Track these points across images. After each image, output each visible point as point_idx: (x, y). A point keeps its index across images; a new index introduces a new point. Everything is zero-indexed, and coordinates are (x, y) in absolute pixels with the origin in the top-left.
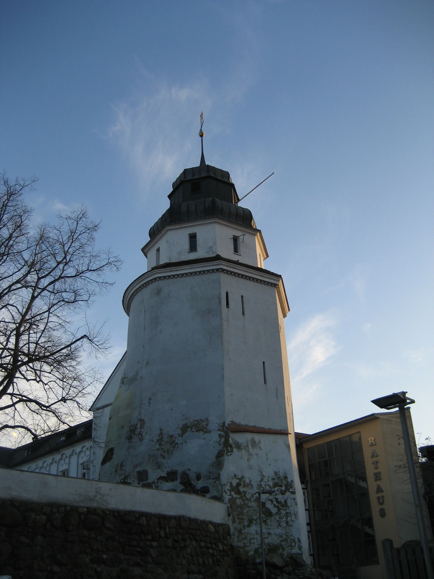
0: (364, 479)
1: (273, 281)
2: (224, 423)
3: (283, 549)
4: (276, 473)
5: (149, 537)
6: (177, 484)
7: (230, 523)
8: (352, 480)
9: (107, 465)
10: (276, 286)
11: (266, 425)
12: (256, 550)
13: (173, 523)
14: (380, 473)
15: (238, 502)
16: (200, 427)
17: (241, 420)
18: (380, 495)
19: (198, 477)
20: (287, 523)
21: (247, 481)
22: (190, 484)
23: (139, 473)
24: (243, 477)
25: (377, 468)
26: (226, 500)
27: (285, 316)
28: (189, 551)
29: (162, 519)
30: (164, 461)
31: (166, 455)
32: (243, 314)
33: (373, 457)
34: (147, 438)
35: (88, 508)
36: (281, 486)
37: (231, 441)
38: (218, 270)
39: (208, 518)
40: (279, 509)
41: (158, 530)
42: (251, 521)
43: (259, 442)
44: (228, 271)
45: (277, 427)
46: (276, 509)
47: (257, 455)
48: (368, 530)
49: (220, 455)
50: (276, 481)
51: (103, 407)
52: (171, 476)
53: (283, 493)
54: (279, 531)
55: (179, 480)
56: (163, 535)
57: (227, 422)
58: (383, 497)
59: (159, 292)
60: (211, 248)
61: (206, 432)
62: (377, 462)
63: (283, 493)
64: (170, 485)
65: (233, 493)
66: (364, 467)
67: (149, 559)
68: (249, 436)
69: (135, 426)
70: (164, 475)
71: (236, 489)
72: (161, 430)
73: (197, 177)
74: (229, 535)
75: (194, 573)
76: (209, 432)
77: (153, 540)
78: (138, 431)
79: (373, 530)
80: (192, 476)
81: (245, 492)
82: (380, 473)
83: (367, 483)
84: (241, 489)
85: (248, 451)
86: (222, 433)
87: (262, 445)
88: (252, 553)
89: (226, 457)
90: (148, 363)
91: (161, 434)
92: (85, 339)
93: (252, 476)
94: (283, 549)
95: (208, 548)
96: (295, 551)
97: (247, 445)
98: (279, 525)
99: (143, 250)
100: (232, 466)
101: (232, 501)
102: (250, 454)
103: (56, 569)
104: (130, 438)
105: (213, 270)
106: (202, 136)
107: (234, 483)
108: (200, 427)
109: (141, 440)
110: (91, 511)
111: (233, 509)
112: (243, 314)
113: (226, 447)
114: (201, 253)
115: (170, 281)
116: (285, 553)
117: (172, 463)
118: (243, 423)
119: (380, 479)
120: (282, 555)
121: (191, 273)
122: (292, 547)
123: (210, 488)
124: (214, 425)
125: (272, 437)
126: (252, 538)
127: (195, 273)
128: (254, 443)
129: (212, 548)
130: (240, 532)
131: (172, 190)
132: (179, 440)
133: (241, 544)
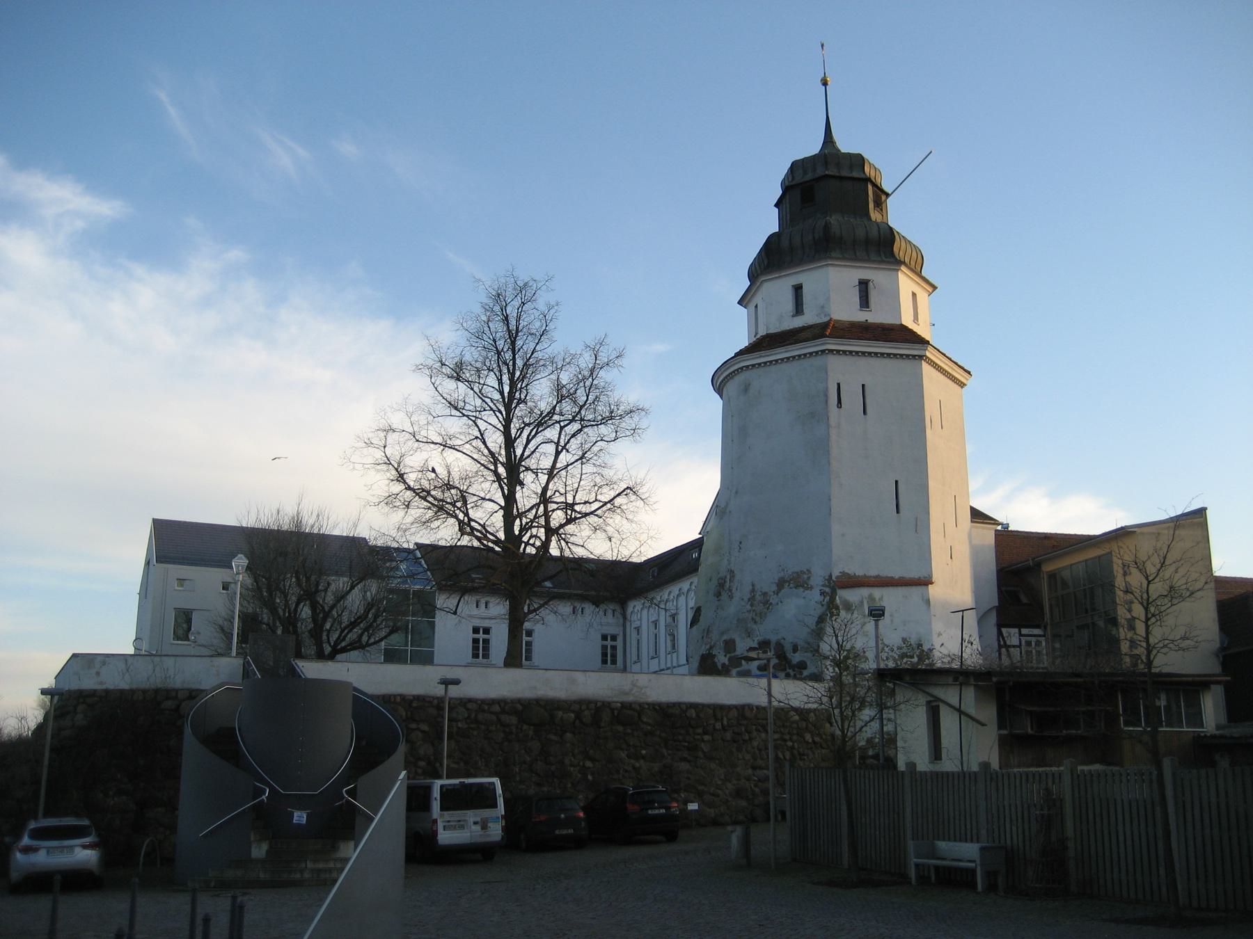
2: (831, 576)
4: (904, 640)
5: (700, 731)
11: (896, 572)
12: (869, 741)
13: (734, 713)
16: (799, 581)
17: (857, 570)
19: (795, 649)
23: (726, 642)
29: (718, 710)
31: (758, 619)
32: (865, 412)
34: (737, 595)
36: (912, 657)
37: (838, 600)
38: (823, 351)
41: (712, 722)
49: (821, 620)
56: (718, 726)
57: (836, 573)
59: (746, 388)
61: (807, 589)
67: (700, 754)
68: (865, 592)
69: (724, 579)
73: (809, 177)
76: (811, 588)
77: (705, 733)
78: (727, 585)
86: (827, 590)
95: (785, 741)
101: (837, 680)
103: (589, 764)
104: (718, 595)
106: (825, 83)
108: (799, 581)
109: (731, 597)
110: (626, 706)
112: (865, 412)
113: (831, 608)
114: (810, 317)
117: (766, 629)
118: (860, 572)
124: (817, 580)
125: (900, 591)
127: (794, 357)
129: (791, 739)
131: (780, 192)
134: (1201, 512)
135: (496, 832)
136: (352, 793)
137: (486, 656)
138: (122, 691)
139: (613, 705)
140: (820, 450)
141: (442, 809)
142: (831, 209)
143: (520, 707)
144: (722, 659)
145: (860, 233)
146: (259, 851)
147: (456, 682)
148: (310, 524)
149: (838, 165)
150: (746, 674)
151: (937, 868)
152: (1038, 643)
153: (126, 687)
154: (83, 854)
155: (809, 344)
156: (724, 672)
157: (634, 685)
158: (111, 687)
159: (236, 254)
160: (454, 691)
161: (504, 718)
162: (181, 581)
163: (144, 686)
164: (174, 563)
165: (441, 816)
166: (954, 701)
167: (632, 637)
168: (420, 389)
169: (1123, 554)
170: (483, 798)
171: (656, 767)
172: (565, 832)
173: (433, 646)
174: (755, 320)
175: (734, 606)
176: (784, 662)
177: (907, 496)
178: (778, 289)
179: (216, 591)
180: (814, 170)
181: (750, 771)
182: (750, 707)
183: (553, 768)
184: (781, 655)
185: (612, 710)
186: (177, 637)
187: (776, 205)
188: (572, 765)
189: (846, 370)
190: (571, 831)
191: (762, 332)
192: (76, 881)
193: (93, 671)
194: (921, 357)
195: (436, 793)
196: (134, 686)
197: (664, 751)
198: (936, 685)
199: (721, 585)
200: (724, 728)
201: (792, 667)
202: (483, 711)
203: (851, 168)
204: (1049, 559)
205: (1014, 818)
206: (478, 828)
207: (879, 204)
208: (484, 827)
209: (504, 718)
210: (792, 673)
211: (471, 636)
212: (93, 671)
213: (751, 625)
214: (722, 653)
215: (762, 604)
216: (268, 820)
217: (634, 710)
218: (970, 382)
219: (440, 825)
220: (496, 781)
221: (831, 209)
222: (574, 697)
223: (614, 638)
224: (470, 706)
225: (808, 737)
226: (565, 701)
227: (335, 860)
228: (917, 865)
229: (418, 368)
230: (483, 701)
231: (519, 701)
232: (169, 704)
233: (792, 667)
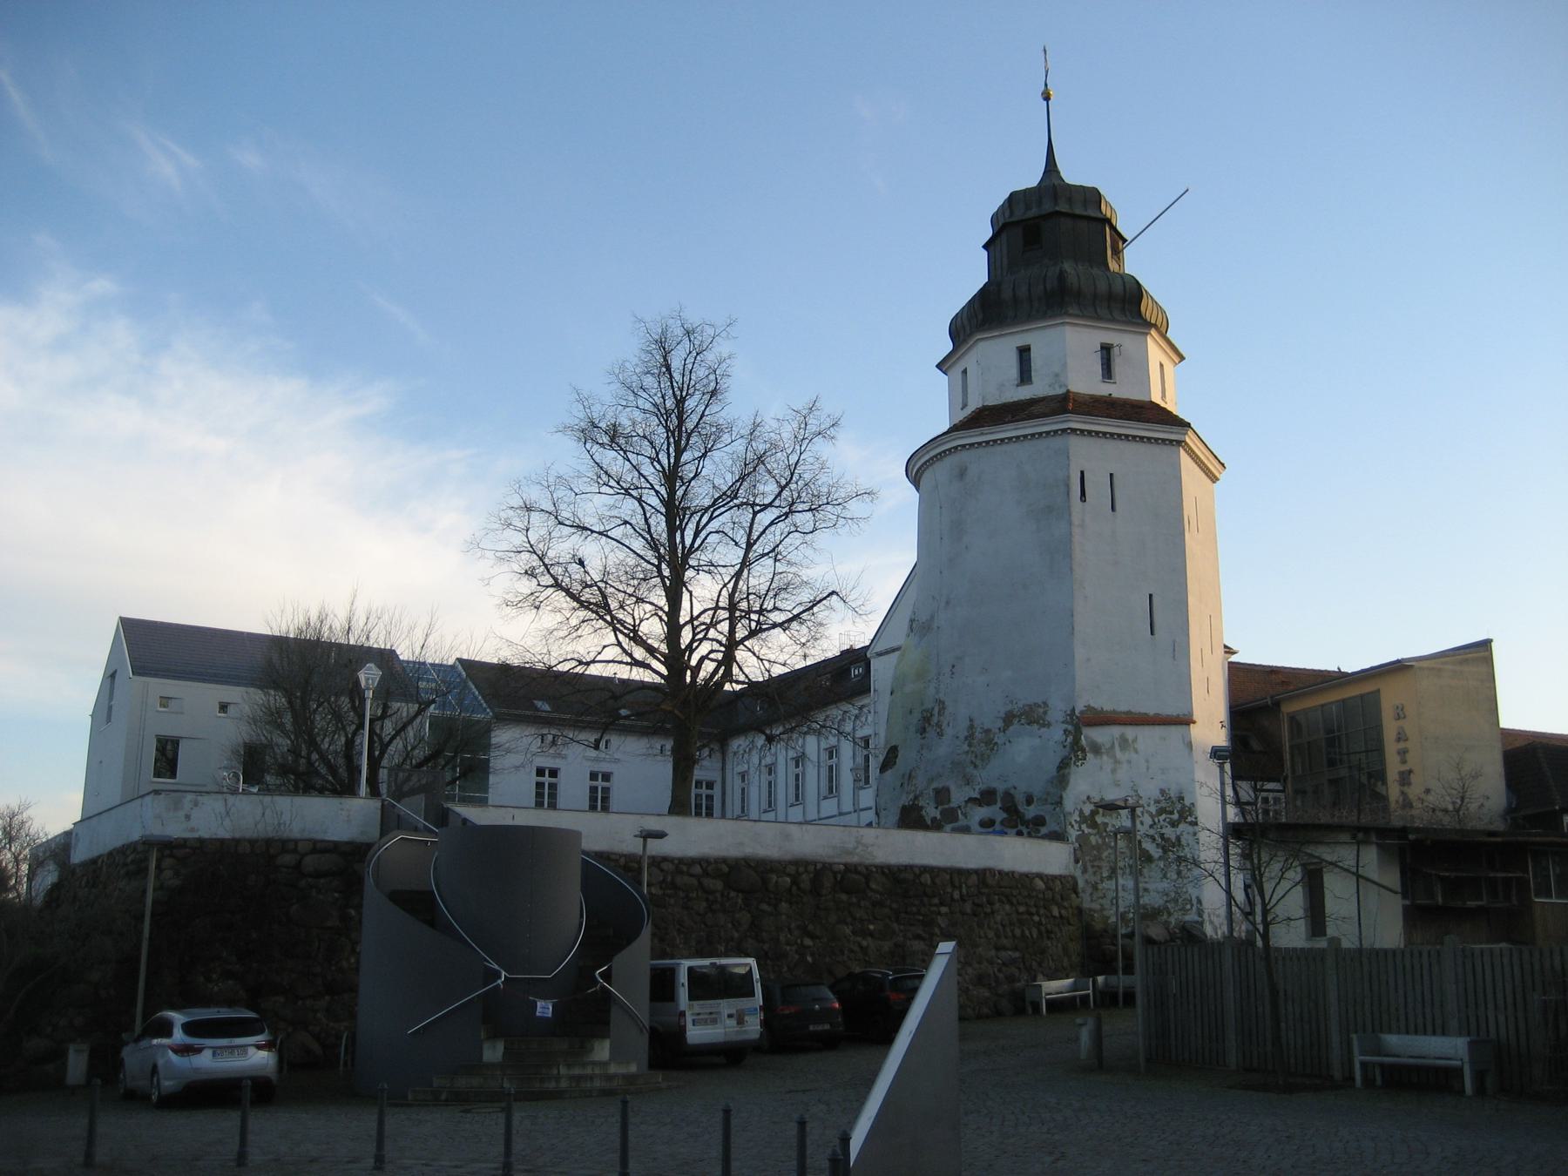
0: (1384, 782)
1: (1173, 437)
3: (1170, 914)
4: (1162, 792)
5: (936, 901)
6: (995, 812)
7: (1078, 874)
9: (889, 772)
11: (1151, 709)
15: (1093, 840)
16: (1033, 716)
17: (1105, 703)
19: (1029, 800)
22: (1017, 811)
25: (1404, 762)
26: (1073, 838)
28: (999, 918)
29: (957, 875)
30: (975, 772)
32: (1113, 509)
34: (949, 732)
35: (845, 865)
38: (1064, 431)
39: (1034, 868)
40: (1165, 851)
43: (1135, 740)
44: (1082, 431)
45: (1170, 710)
47: (1129, 762)
49: (1064, 765)
50: (1163, 805)
51: (887, 652)
52: (987, 797)
53: (1174, 824)
54: (1165, 885)
55: (999, 804)
56: (956, 895)
57: (1080, 707)
59: (962, 473)
60: (1057, 375)
61: (1044, 726)
63: (1174, 824)
64: (982, 813)
65: (1084, 827)
67: (937, 930)
68: (1116, 731)
73: (1034, 212)
74: (1076, 893)
75: (1005, 948)
76: (1049, 725)
77: (942, 904)
78: (935, 719)
80: (1020, 798)
81: (1106, 825)
86: (1070, 728)
87: (1140, 745)
90: (948, 603)
91: (971, 727)
92: (835, 597)
94: (1170, 914)
95: (1031, 914)
96: (1191, 917)
98: (1165, 876)
100: (1086, 784)
101: (1083, 839)
102: (1117, 762)
103: (808, 942)
106: (1047, 98)
107: (1087, 809)
108: (1033, 716)
109: (940, 734)
110: (850, 869)
112: (1113, 509)
114: (1040, 387)
115: (981, 451)
116: (1173, 920)
117: (988, 776)
118: (1108, 707)
119: (1409, 784)
120: (1167, 923)
124: (1057, 713)
125: (1159, 731)
127: (1025, 436)
128: (1124, 743)
133: (1095, 906)
134: (1486, 645)
135: (753, 1028)
136: (607, 976)
137: (605, 809)
138: (222, 841)
139: (836, 868)
140: (1059, 554)
141: (691, 998)
142: (1054, 254)
143: (725, 869)
144: (931, 812)
145: (1102, 286)
146: (493, 1052)
147: (660, 835)
148: (334, 631)
149: (1070, 200)
150: (966, 830)
151: (1382, 1065)
152: (1277, 800)
153: (227, 836)
154: (256, 1057)
156: (936, 826)
157: (858, 842)
158: (206, 836)
159: (102, 285)
160: (656, 847)
161: (707, 882)
162: (165, 701)
163: (249, 834)
164: (156, 676)
165: (691, 1007)
166: (1350, 862)
167: (734, 785)
168: (571, 457)
169: (1391, 695)
170: (736, 987)
171: (887, 946)
172: (820, 1028)
173: (486, 791)
174: (962, 391)
175: (945, 748)
176: (1017, 816)
177: (1163, 612)
178: (995, 355)
179: (215, 718)
180: (1040, 203)
181: (993, 953)
182: (991, 871)
183: (766, 947)
184: (1011, 808)
185: (835, 873)
186: (158, 774)
187: (985, 247)
188: (788, 944)
189: (1094, 456)
190: (827, 1027)
191: (973, 405)
192: (261, 1091)
193: (181, 814)
194: (1179, 443)
195: (683, 977)
196: (237, 835)
197: (895, 926)
198: (1321, 843)
199: (927, 719)
200: (962, 899)
201: (1026, 823)
202: (682, 872)
203: (1085, 204)
204: (1290, 699)
205: (1501, 1002)
206: (733, 1022)
207: (1117, 253)
208: (740, 1022)
209: (707, 882)
210: (1025, 831)
211: (588, 783)
212: (181, 814)
213: (970, 769)
214: (933, 805)
215: (983, 744)
216: (499, 1014)
217: (859, 873)
218: (1223, 476)
219: (689, 1019)
220: (752, 961)
221: (1054, 254)
222: (788, 857)
223: (710, 785)
224: (665, 866)
225: (1056, 912)
226: (779, 862)
227: (594, 1063)
228: (1364, 1065)
229: (565, 429)
230: (681, 861)
231: (724, 860)
232: (288, 859)
233: (1026, 823)
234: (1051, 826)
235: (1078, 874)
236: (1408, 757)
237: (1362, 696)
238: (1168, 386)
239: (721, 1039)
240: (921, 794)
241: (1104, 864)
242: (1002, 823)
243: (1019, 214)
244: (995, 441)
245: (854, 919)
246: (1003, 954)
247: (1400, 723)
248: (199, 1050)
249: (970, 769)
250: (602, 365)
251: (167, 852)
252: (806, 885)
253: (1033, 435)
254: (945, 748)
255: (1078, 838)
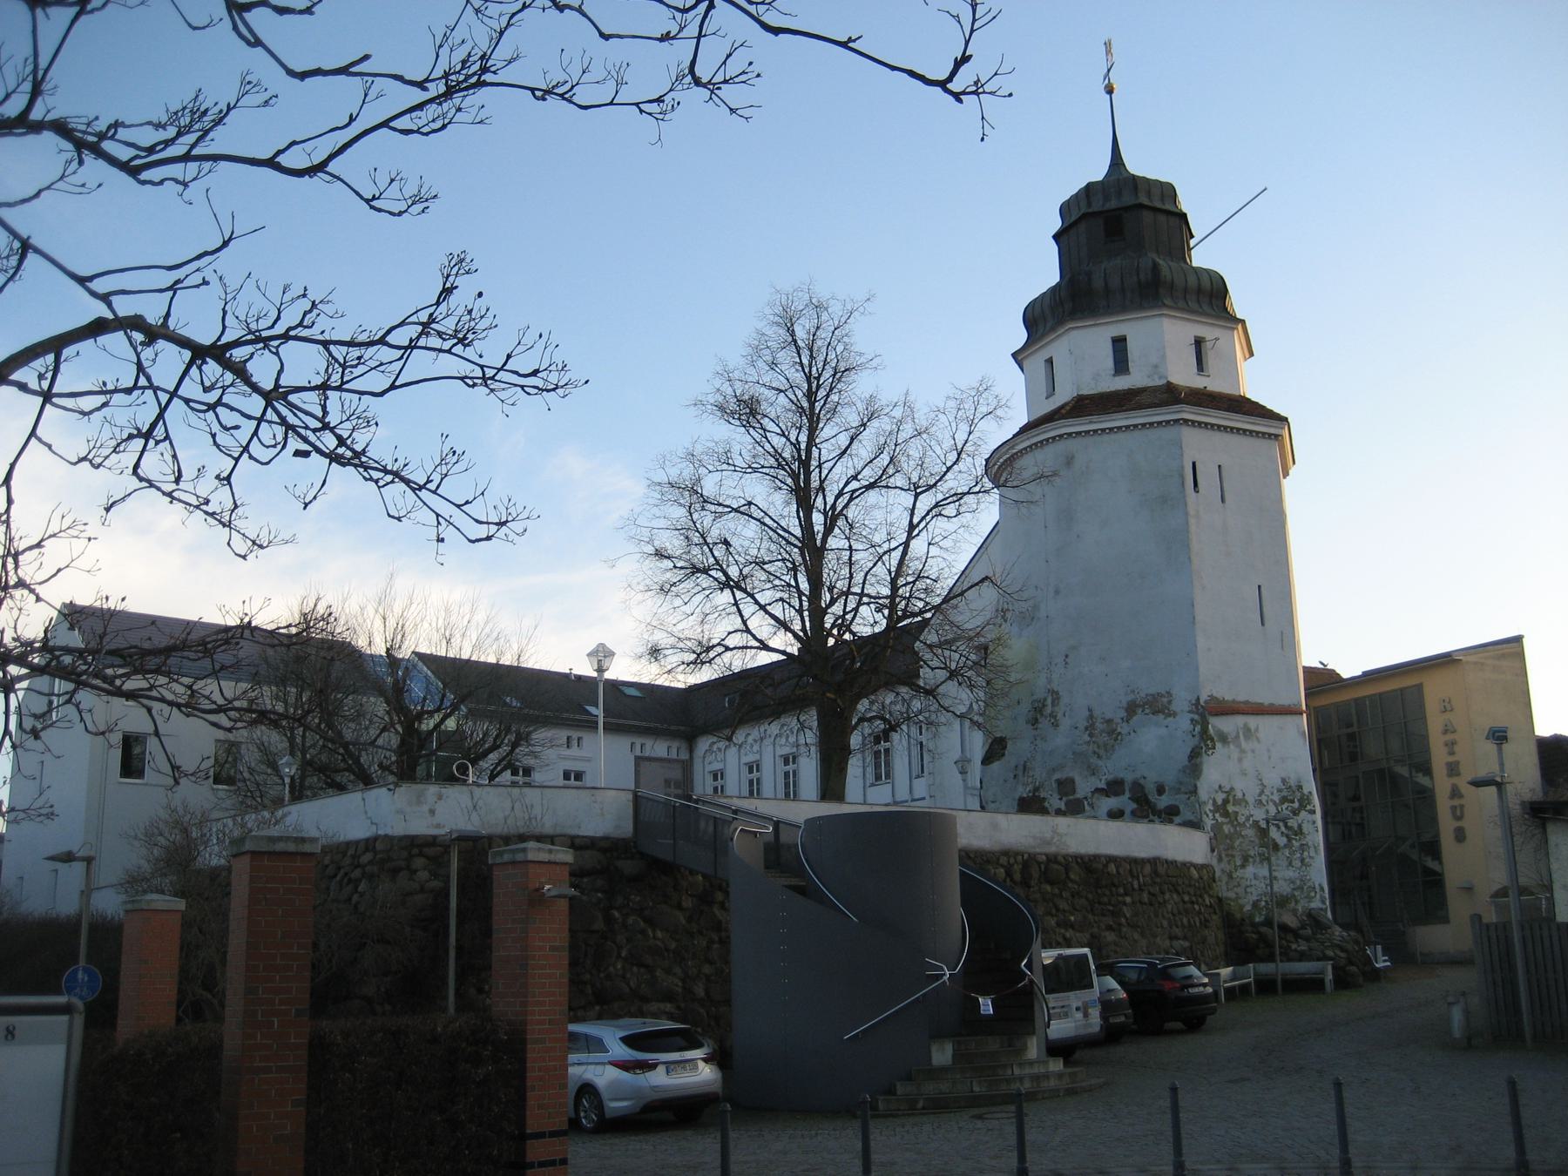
0: (1427, 770)
1: (1272, 431)
3: (1297, 902)
4: (1284, 781)
6: (1123, 801)
7: (1214, 862)
8: (1403, 771)
9: (996, 766)
10: (1277, 437)
11: (1264, 697)
12: (1255, 904)
14: (1458, 763)
15: (1226, 829)
16: (1158, 706)
17: (1226, 693)
18: (1456, 802)
19: (1161, 790)
20: (1302, 860)
21: (1240, 795)
22: (1147, 802)
23: (1060, 783)
24: (1232, 789)
25: (1452, 753)
26: (1208, 828)
27: (1286, 474)
29: (1135, 864)
30: (1100, 763)
31: (1102, 752)
33: (1445, 732)
34: (1065, 723)
38: (1176, 421)
40: (1289, 840)
42: (1246, 859)
43: (1257, 729)
44: (1193, 422)
46: (1285, 840)
48: (1431, 864)
49: (1195, 754)
50: (1285, 793)
52: (1115, 787)
53: (1295, 813)
54: (1290, 874)
55: (1127, 795)
58: (1462, 806)
62: (1453, 743)
64: (1111, 803)
66: (1427, 750)
68: (1240, 720)
70: (1102, 785)
71: (1221, 809)
72: (1090, 710)
75: (1177, 938)
76: (1174, 715)
77: (1126, 894)
78: (1049, 710)
79: (1441, 863)
80: (1150, 788)
82: (1458, 763)
83: (1432, 778)
84: (1230, 808)
85: (1239, 746)
86: (1196, 717)
87: (1261, 735)
88: (1248, 907)
89: (1205, 757)
90: (1057, 592)
91: (1091, 717)
93: (1245, 787)
97: (1237, 737)
98: (1290, 864)
99: (1014, 355)
100: (1217, 772)
101: (1217, 828)
102: (1243, 751)
105: (1168, 422)
107: (1220, 798)
108: (1158, 706)
109: (1056, 725)
110: (1052, 859)
111: (1217, 842)
113: (1204, 741)
117: (1114, 766)
119: (1458, 774)
120: (1294, 912)
121: (1127, 427)
122: (1310, 899)
123: (1181, 807)
124: (1181, 702)
126: (1251, 885)
127: (1135, 426)
128: (1248, 733)
130: (1230, 876)
132: (1123, 729)
133: (1231, 895)
134: (1518, 640)
140: (1177, 544)
142: (1124, 247)
144: (1055, 802)
146: (942, 1055)
149: (1149, 194)
155: (1158, 411)
157: (1054, 832)
169: (1435, 689)
176: (1145, 805)
180: (1119, 194)
181: (1167, 942)
185: (1039, 863)
187: (1057, 237)
189: (1202, 447)
191: (1064, 395)
206: (1079, 1015)
208: (1086, 1015)
212: (425, 808)
213: (1094, 760)
214: (1056, 796)
221: (1124, 247)
222: (996, 848)
234: (1187, 815)
235: (1214, 862)
236: (1456, 748)
237: (1402, 690)
238: (1255, 383)
239: (1072, 1034)
240: (1042, 785)
241: (1237, 853)
242: (1133, 813)
243: (1097, 206)
244: (1103, 430)
245: (1058, 910)
246: (1175, 943)
247: (1448, 716)
248: (653, 1067)
249: (1094, 760)
250: (725, 338)
251: (415, 851)
252: (1017, 877)
253: (1144, 425)
254: (1061, 739)
255: (1213, 827)
